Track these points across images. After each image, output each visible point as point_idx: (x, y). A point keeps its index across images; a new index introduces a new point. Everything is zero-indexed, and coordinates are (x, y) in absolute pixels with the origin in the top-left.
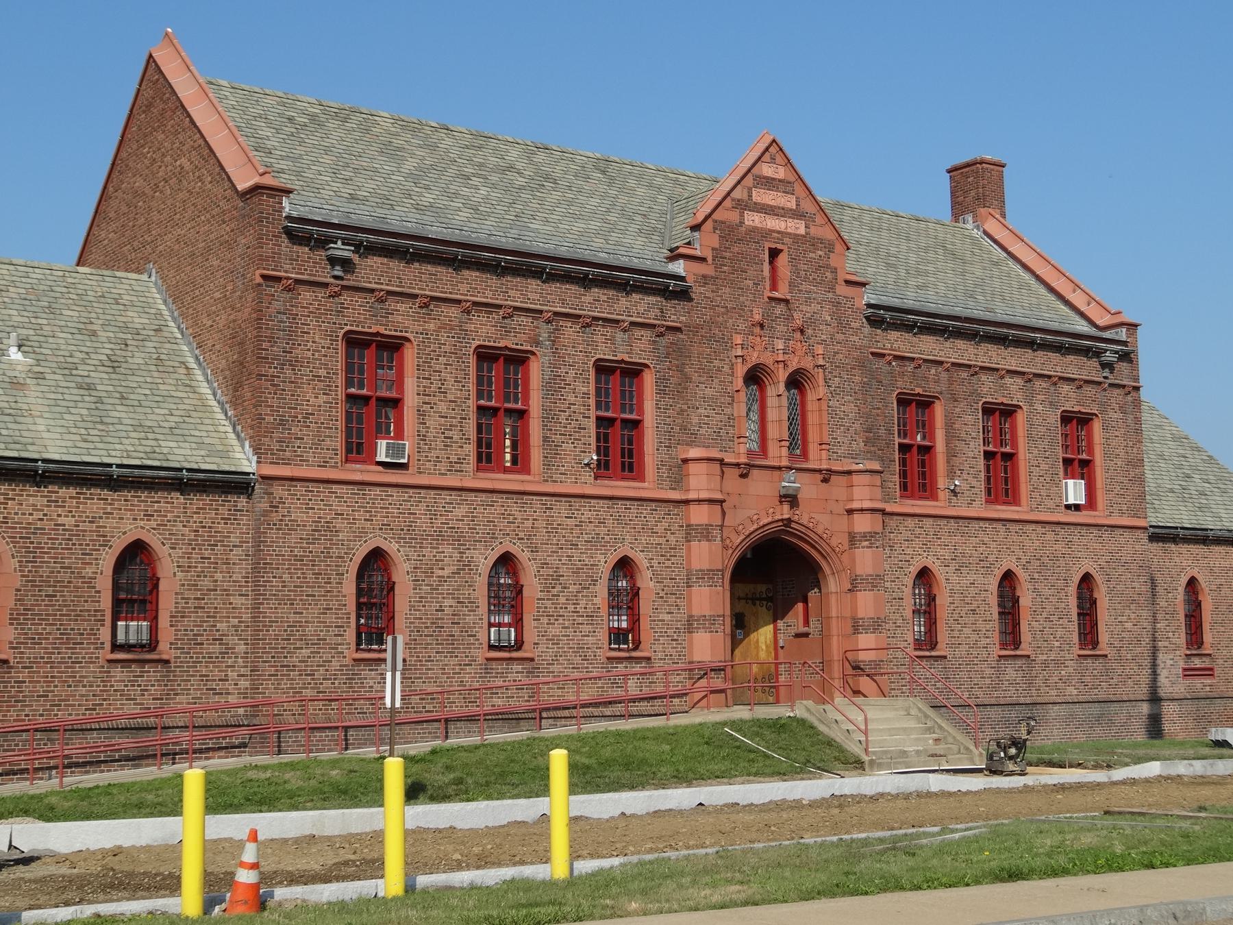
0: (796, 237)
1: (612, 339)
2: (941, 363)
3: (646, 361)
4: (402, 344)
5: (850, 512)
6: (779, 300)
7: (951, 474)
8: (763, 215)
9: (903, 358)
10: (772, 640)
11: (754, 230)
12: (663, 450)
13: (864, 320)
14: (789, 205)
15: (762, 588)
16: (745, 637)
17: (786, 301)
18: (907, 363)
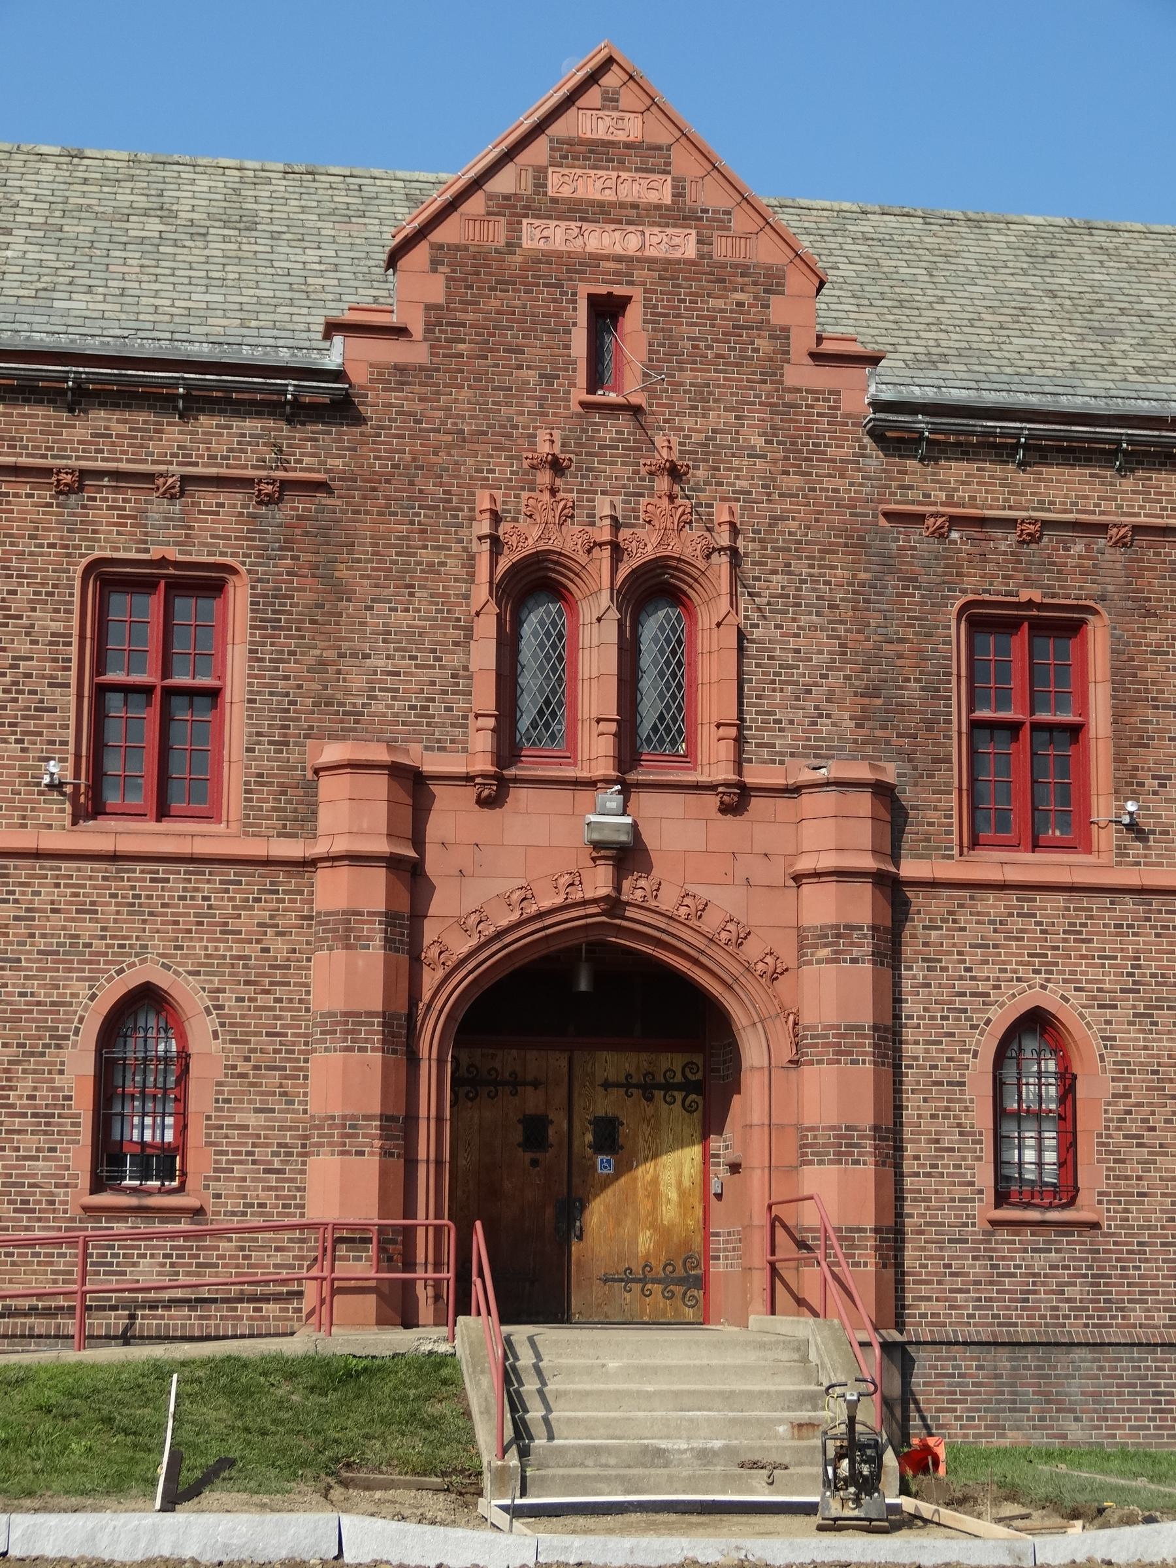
0: (668, 268)
1: (139, 517)
2: (1102, 528)
3: (228, 560)
4: (1084, 622)
5: (798, 878)
6: (613, 408)
7: (1129, 785)
8: (573, 224)
9: (982, 522)
10: (698, 1180)
11: (548, 257)
12: (265, 749)
13: (867, 440)
14: (653, 197)
15: (672, 1063)
16: (617, 1176)
17: (636, 410)
18: (998, 533)
